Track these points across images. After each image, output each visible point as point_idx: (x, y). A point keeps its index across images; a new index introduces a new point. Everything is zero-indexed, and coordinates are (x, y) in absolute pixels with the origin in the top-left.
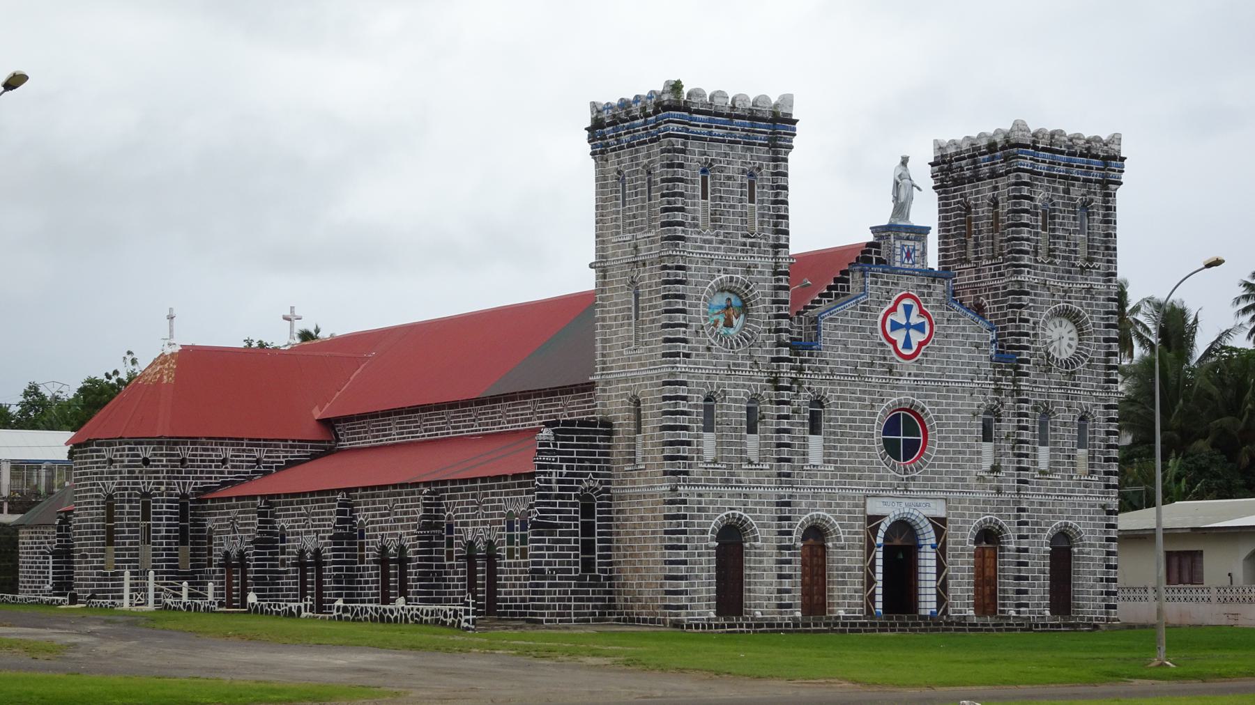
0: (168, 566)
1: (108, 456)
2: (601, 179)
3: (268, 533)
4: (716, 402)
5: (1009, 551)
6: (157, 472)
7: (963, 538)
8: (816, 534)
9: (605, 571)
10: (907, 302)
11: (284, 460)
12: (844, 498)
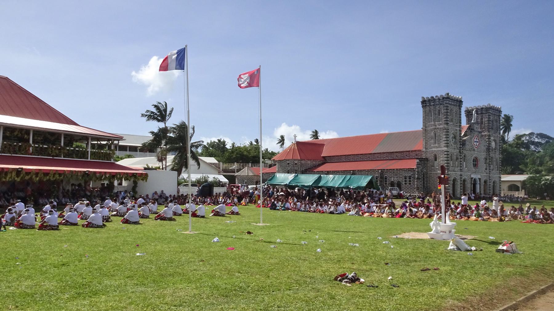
1: (288, 163)
2: (425, 112)
7: (482, 181)
8: (464, 181)
10: (476, 137)
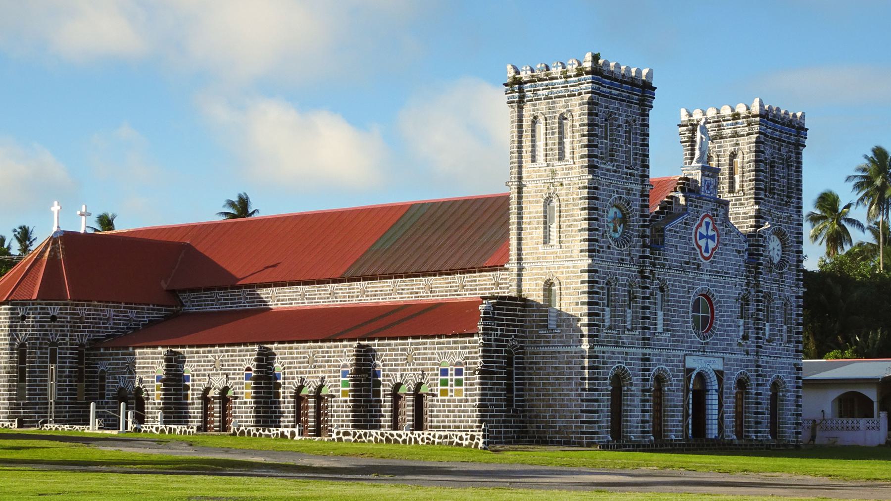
0: (70, 399)
3: (173, 375)
4: (611, 285)
5: (752, 394)
6: (63, 326)
7: (731, 384)
8: (660, 379)
9: (519, 406)
11: (147, 320)
12: (674, 356)
